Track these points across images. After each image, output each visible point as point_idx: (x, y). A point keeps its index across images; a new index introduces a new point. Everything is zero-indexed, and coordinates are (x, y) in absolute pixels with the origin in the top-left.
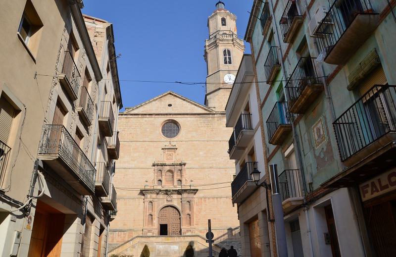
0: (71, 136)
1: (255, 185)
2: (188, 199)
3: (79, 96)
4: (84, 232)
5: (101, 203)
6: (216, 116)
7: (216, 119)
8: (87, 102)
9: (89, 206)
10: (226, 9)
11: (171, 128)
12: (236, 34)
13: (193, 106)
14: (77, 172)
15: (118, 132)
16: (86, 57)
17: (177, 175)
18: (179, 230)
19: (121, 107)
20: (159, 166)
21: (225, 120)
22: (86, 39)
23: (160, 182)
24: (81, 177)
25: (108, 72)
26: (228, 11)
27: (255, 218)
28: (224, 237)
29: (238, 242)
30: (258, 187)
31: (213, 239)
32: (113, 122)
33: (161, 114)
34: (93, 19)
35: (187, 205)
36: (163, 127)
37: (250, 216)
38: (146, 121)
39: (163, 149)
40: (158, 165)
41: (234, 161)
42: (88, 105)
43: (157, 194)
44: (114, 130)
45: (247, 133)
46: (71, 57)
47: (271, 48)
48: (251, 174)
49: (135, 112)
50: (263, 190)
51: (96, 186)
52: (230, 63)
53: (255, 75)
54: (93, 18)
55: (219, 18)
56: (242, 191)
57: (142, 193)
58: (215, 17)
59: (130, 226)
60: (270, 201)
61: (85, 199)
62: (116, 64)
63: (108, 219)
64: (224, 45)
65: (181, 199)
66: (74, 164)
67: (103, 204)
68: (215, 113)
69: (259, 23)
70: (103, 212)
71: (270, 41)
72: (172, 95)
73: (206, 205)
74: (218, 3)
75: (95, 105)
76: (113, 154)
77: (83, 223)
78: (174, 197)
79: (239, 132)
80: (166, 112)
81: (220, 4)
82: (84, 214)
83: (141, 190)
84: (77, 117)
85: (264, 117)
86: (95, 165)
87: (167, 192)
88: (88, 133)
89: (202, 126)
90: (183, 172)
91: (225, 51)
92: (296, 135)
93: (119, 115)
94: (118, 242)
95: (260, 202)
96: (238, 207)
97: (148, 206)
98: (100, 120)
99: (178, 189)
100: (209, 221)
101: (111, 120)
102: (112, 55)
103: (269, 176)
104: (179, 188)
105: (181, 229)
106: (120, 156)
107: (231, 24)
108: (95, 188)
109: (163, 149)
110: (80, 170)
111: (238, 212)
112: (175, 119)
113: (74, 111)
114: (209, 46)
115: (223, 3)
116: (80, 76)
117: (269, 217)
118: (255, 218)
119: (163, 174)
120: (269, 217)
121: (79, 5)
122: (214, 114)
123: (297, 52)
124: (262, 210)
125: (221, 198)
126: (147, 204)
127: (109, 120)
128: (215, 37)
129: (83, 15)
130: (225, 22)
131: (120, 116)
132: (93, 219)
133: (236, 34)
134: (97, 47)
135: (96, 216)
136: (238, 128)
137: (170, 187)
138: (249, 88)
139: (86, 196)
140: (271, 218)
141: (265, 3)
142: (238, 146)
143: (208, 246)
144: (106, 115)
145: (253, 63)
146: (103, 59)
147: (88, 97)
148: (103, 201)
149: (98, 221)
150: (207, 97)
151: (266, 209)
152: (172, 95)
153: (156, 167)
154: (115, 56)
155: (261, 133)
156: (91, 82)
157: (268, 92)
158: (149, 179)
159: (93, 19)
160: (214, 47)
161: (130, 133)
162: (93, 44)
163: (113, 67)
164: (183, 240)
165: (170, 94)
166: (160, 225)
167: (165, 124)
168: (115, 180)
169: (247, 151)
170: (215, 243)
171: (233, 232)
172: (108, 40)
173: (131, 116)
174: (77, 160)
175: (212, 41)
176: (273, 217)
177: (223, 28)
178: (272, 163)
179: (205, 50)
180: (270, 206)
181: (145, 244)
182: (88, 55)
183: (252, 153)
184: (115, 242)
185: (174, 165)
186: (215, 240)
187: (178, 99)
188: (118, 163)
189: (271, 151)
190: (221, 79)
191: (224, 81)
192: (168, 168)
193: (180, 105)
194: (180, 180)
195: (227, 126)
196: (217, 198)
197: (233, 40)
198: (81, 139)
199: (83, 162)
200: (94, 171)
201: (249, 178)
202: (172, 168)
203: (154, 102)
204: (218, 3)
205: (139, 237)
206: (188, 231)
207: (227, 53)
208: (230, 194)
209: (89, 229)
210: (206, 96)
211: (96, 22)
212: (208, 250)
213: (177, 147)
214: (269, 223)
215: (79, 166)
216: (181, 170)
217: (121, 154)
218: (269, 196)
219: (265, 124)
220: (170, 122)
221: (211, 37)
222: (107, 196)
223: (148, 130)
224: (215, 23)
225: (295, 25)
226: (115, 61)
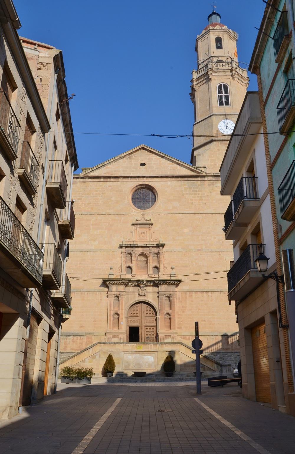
0: (9, 209)
1: (261, 276)
2: (168, 294)
3: (19, 155)
4: (28, 337)
5: (50, 297)
6: (206, 179)
7: (207, 183)
8: (30, 162)
9: (35, 303)
10: (223, 23)
11: (145, 195)
12: (237, 61)
13: (175, 165)
14: (19, 257)
15: (72, 203)
16: (27, 99)
17: (153, 260)
18: (155, 335)
19: (76, 167)
20: (128, 248)
21: (218, 185)
22: (26, 74)
23: (129, 269)
24: (24, 264)
25: (57, 120)
26: (225, 27)
27: (262, 321)
28: (216, 346)
29: (236, 354)
30: (265, 279)
31: (201, 349)
32: (66, 189)
33: (131, 177)
34: (35, 44)
35: (166, 301)
36: (134, 194)
37: (253, 318)
38: (110, 186)
39: (133, 225)
40: (126, 247)
41: (231, 242)
42: (32, 166)
43: (126, 285)
44: (67, 200)
45: (250, 203)
46: (6, 100)
47: (288, 81)
48: (256, 261)
49: (92, 174)
50: (272, 284)
51: (44, 275)
52: (227, 103)
53: (263, 122)
54: (34, 42)
55: (212, 37)
56: (242, 284)
57: (105, 284)
58: (206, 37)
59: (89, 329)
60: (282, 298)
61: (29, 293)
62: (68, 108)
63: (59, 320)
64: (219, 77)
65: (158, 293)
66: (15, 247)
67: (54, 299)
68: (205, 174)
69: (270, 45)
70: (53, 309)
71: (286, 72)
72: (146, 150)
73: (192, 301)
74: (210, 15)
75: (41, 165)
76: (66, 232)
77: (26, 325)
78: (148, 290)
79: (239, 202)
80: (138, 174)
81: (214, 16)
82: (28, 313)
83: (104, 281)
84: (18, 184)
85: (275, 182)
86: (42, 246)
87: (139, 283)
88: (32, 204)
89: (187, 194)
90: (161, 256)
91: (220, 87)
93: (74, 178)
94: (72, 349)
95: (267, 300)
96: (237, 306)
97: (113, 301)
98: (48, 185)
99: (153, 279)
100: (197, 324)
101: (62, 186)
102: (63, 96)
103: (281, 265)
104: (155, 277)
105: (157, 334)
106: (75, 235)
107: (230, 46)
108: (43, 278)
109: (133, 225)
110: (23, 254)
111: (237, 313)
113: (13, 175)
114: (197, 79)
115: (218, 15)
116: (20, 126)
117: (281, 322)
118: (262, 321)
119: (134, 258)
120: (281, 322)
121: (14, 23)
122: (204, 177)
124: (271, 311)
125: (212, 292)
126: (111, 298)
127: (60, 185)
128: (207, 66)
129: (20, 37)
130: (221, 44)
131: (75, 180)
132: (39, 319)
133: (237, 61)
134: (42, 85)
135: (43, 315)
136: (238, 197)
137: (142, 276)
138: (253, 142)
139: (30, 289)
140: (284, 323)
141: (282, 12)
142: (237, 222)
143: (195, 358)
144: (56, 180)
145: (260, 104)
146: (50, 101)
147: (31, 155)
148: (53, 296)
149: (47, 322)
150: (196, 153)
151: (275, 310)
152: (146, 150)
153: (124, 249)
154: (67, 98)
156: (35, 134)
158: (115, 265)
159: (35, 44)
160: (204, 82)
161: (89, 203)
162: (37, 80)
163: (63, 112)
164: (160, 348)
165: (143, 148)
166: (130, 327)
167: (136, 191)
168: (69, 267)
169: (250, 229)
170: (205, 353)
171: (230, 340)
172: (56, 75)
173: (90, 180)
174: (18, 241)
175: (202, 72)
176: (287, 321)
177: (219, 52)
178: (287, 246)
179: (193, 86)
180: (282, 306)
181: (109, 353)
182: (30, 96)
183: (257, 232)
184: (68, 350)
185: (149, 247)
186: (204, 350)
187: (154, 155)
188: (72, 244)
189: (284, 230)
190: (214, 127)
191: (218, 131)
192: (140, 250)
193: (156, 165)
194: (157, 268)
195: (223, 193)
196: (207, 292)
197: (231, 71)
198: (23, 213)
199: (27, 243)
200: (41, 255)
201: (252, 267)
202: (146, 251)
203: (121, 160)
204: (210, 15)
206: (167, 336)
207: (223, 89)
208: (226, 287)
209: (35, 333)
210: (193, 151)
211: (39, 49)
212: (195, 363)
213: (152, 222)
214: (280, 329)
215: (22, 249)
216: (158, 254)
217: (77, 231)
218: (281, 291)
219: (276, 192)
220: (143, 188)
221: (200, 67)
222: (58, 289)
223: (113, 198)
224: (207, 47)
226: (68, 104)
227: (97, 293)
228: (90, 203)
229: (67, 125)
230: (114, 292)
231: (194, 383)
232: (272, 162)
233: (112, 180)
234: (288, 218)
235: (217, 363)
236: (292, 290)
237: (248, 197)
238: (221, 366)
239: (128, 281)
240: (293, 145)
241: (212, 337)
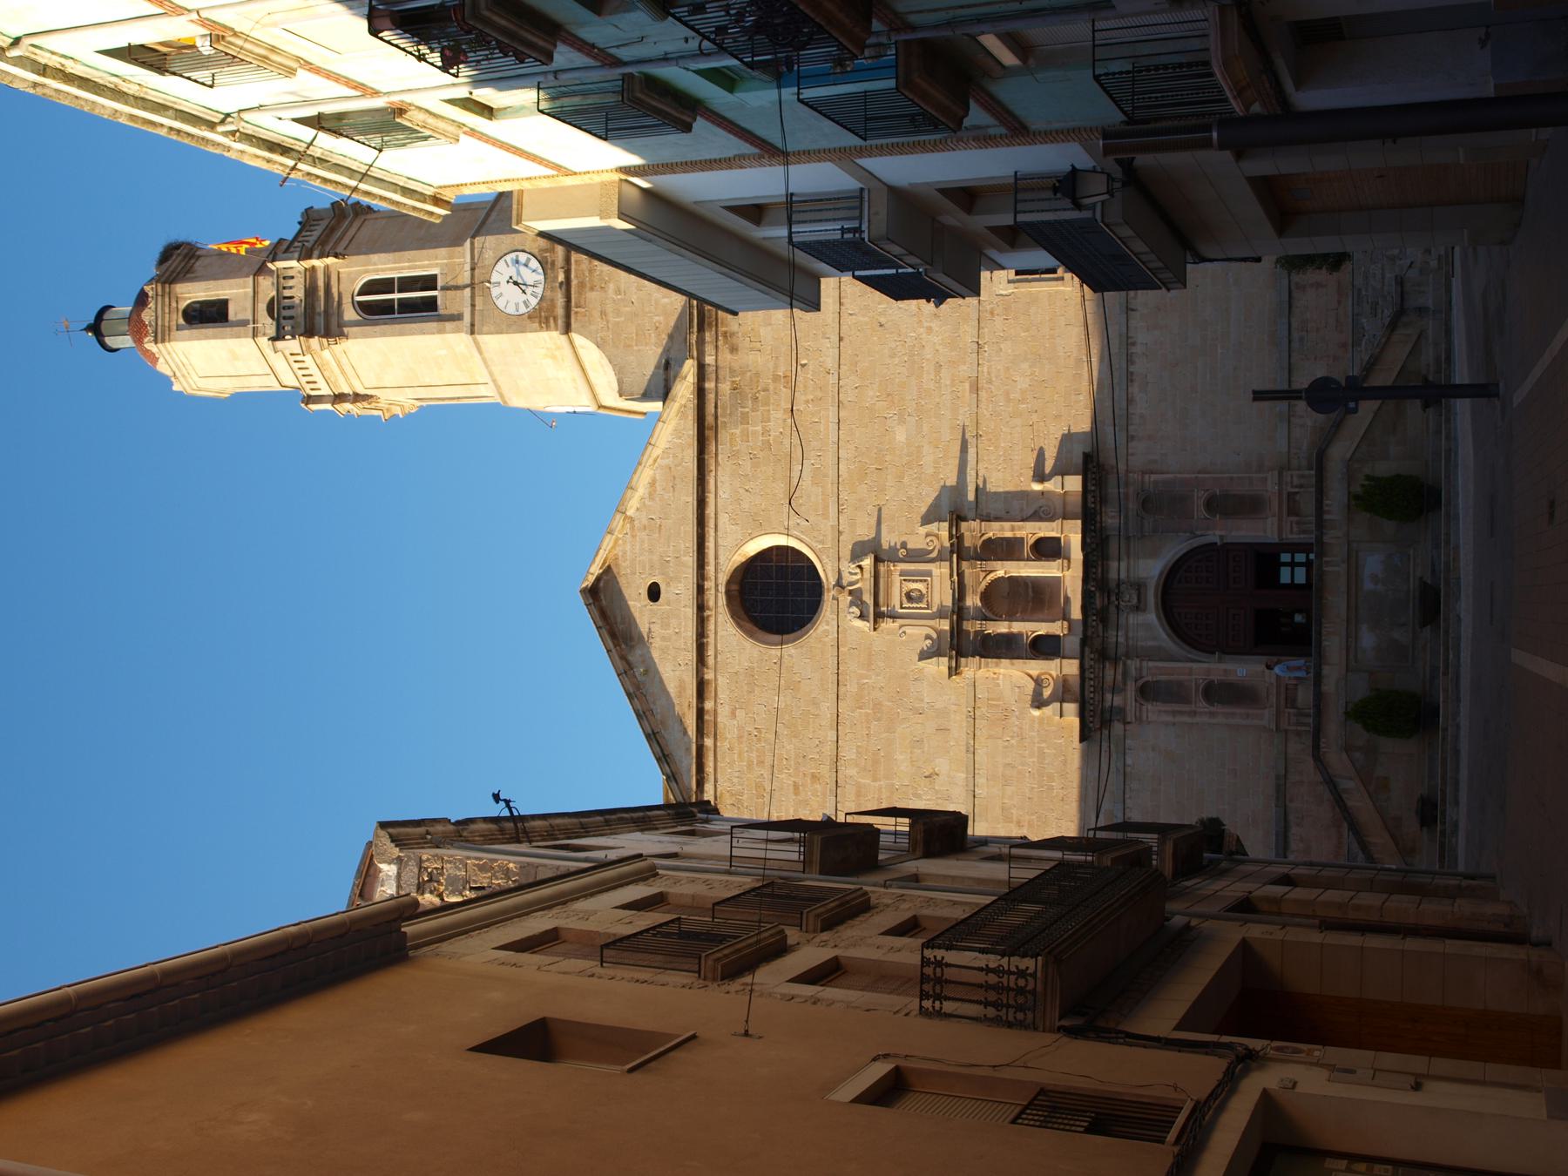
6: (709, 360)
30: (1132, 178)
33: (701, 634)
38: (733, 714)
41: (985, 275)
56: (1139, 246)
79: (868, 252)
80: (690, 612)
89: (766, 432)
92: (949, 24)
102: (502, 831)
112: (723, 579)
123: (599, 14)
155: (879, 159)
157: (731, 122)
183: (967, 196)
205: (1316, 747)
225: (496, 18)
227: (1129, 761)
228: (796, 786)
229: (582, 826)
230: (1125, 700)
231: (1463, 408)
232: (757, 151)
233: (708, 705)
234: (961, 113)
235: (1393, 326)
236: (1215, 135)
237: (855, 224)
238: (1401, 312)
239: (1087, 650)
240: (726, 93)
241: (1295, 345)
